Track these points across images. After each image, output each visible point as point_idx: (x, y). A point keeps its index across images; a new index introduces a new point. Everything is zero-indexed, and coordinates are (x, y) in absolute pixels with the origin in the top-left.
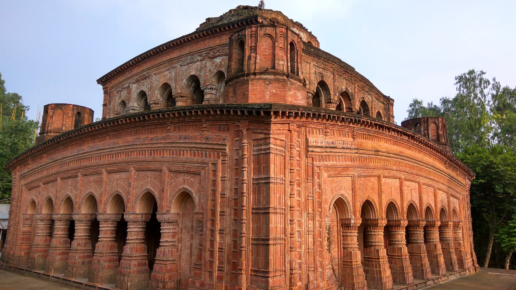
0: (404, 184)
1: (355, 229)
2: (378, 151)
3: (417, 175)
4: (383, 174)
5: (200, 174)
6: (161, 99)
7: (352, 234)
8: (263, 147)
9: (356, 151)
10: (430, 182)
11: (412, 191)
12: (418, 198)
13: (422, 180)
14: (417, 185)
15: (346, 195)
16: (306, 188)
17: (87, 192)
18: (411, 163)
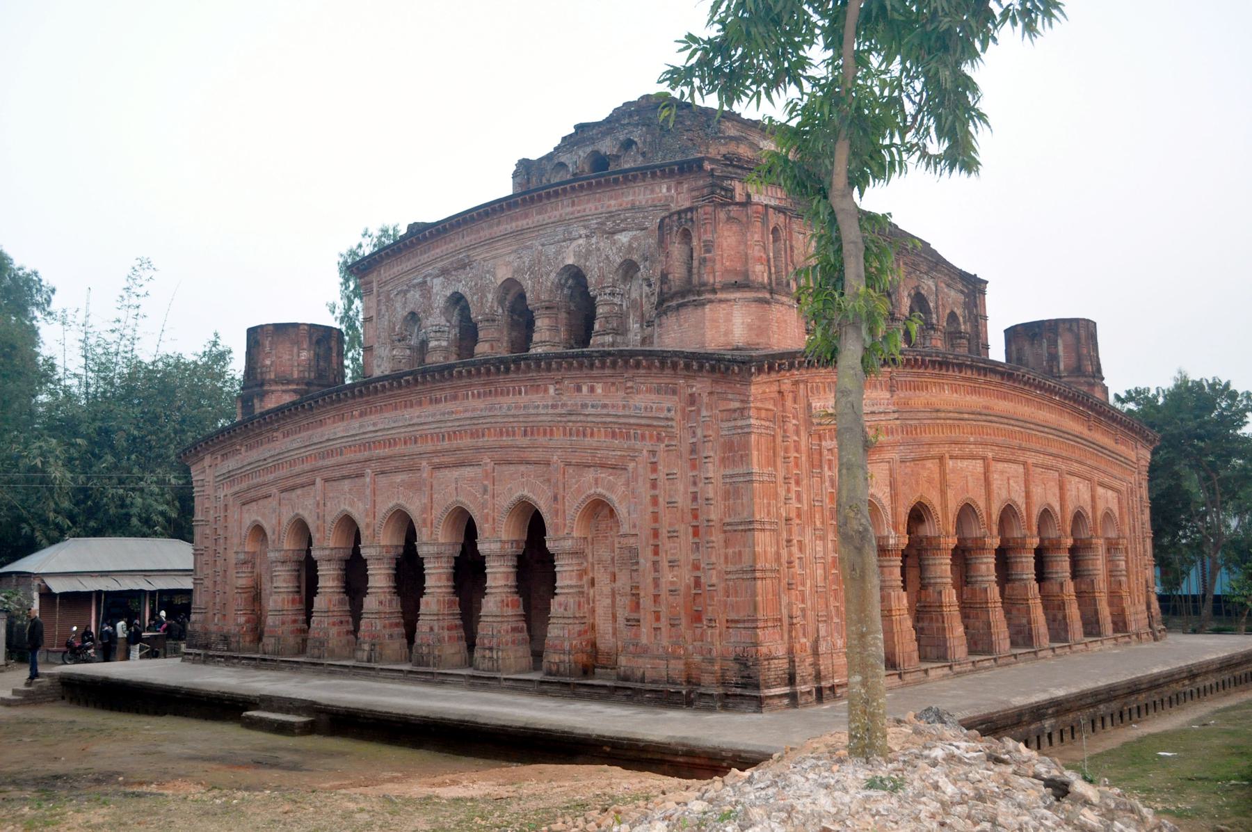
0: (992, 469)
1: (897, 555)
2: (938, 411)
3: (1021, 448)
4: (948, 452)
5: (625, 469)
6: (500, 311)
7: (892, 563)
8: (740, 423)
9: (896, 415)
10: (1049, 461)
11: (1011, 482)
12: (1023, 494)
13: (1032, 459)
14: (1021, 469)
15: (880, 495)
16: (810, 487)
17: (391, 505)
18: (1006, 426)
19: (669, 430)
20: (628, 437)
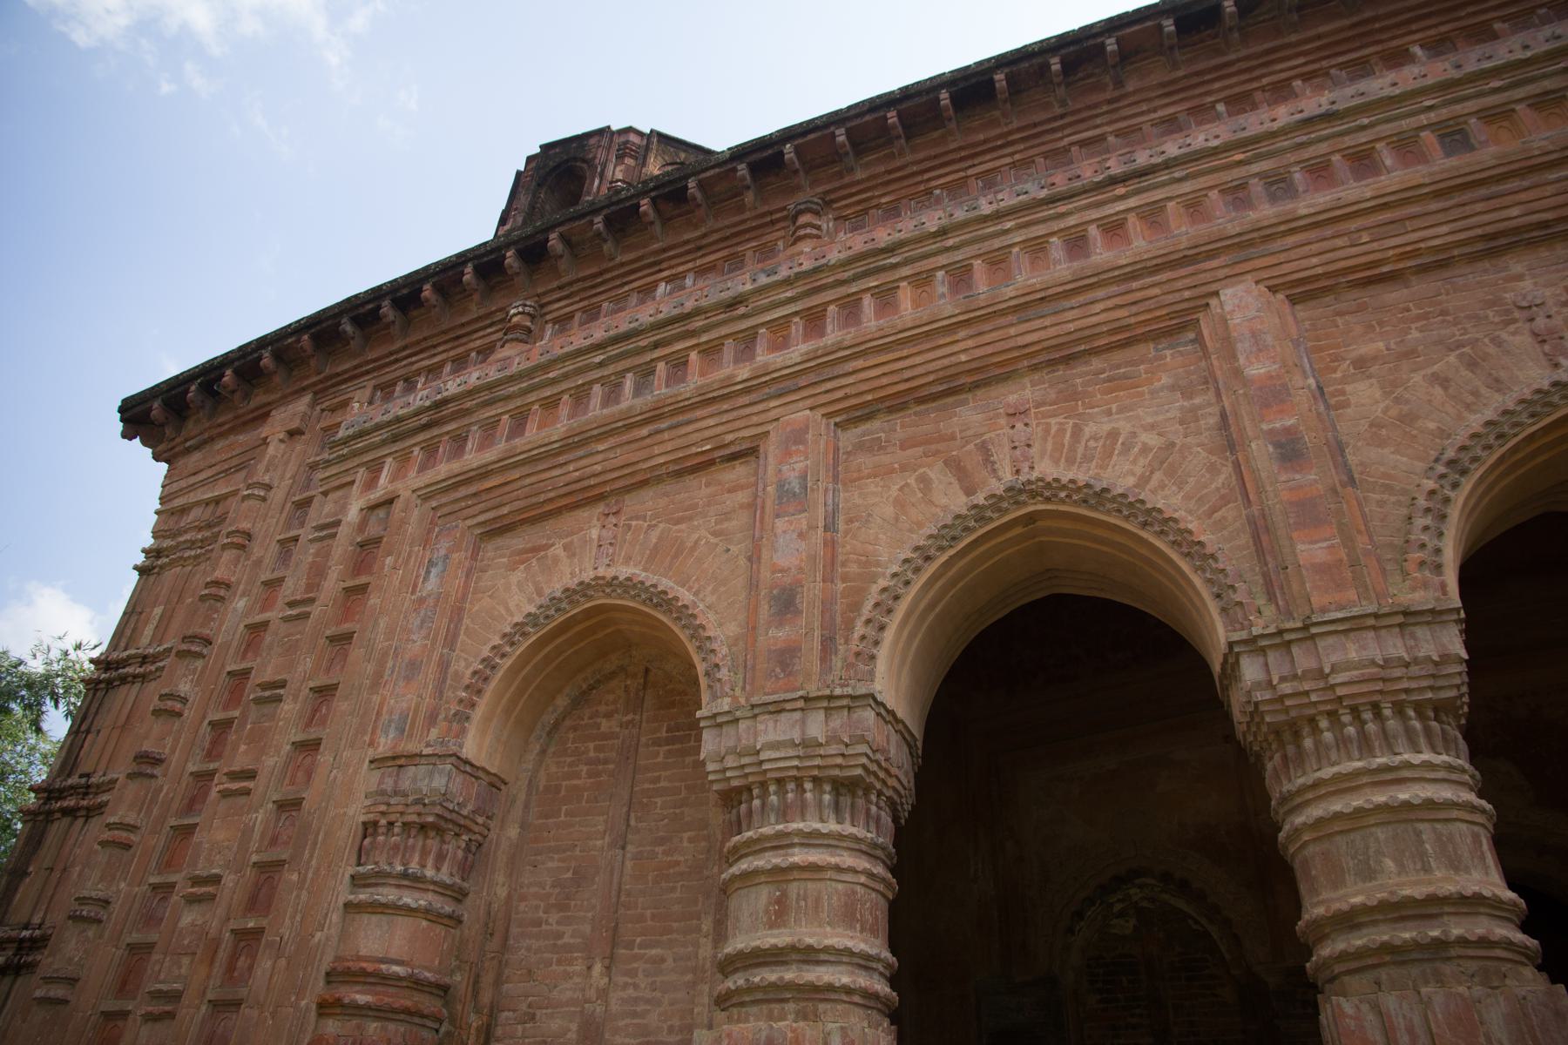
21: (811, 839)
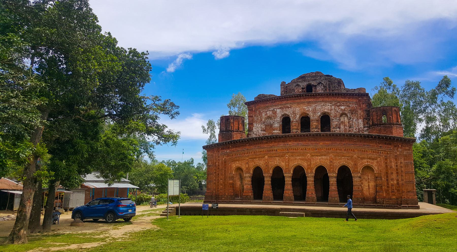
19: (391, 152)
20: (378, 153)
21: (248, 179)
